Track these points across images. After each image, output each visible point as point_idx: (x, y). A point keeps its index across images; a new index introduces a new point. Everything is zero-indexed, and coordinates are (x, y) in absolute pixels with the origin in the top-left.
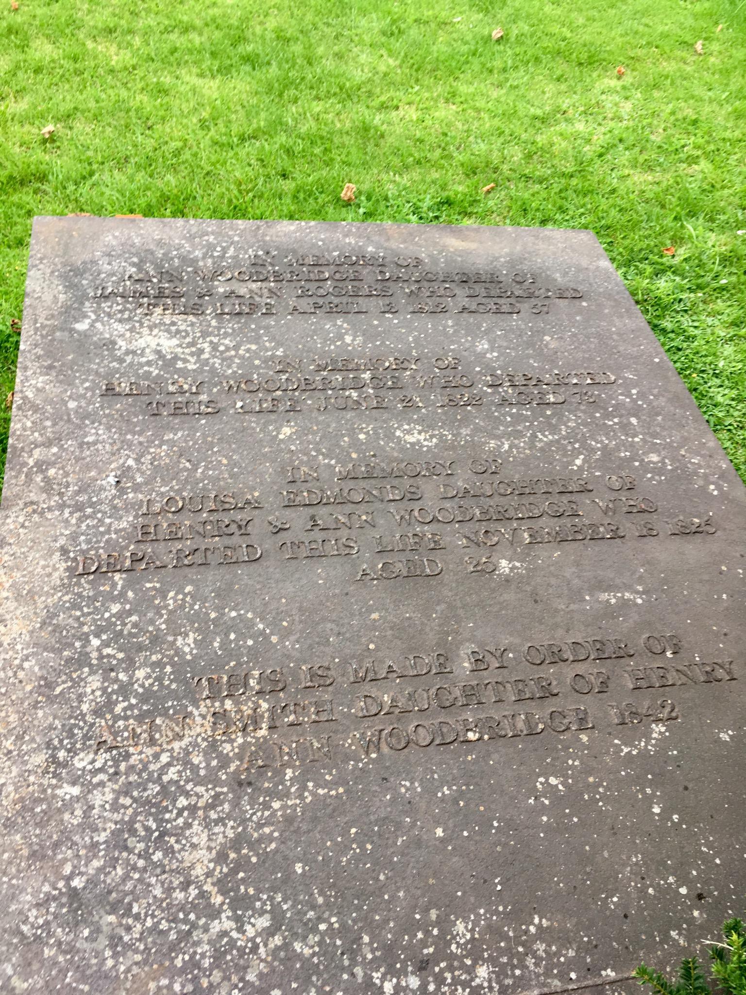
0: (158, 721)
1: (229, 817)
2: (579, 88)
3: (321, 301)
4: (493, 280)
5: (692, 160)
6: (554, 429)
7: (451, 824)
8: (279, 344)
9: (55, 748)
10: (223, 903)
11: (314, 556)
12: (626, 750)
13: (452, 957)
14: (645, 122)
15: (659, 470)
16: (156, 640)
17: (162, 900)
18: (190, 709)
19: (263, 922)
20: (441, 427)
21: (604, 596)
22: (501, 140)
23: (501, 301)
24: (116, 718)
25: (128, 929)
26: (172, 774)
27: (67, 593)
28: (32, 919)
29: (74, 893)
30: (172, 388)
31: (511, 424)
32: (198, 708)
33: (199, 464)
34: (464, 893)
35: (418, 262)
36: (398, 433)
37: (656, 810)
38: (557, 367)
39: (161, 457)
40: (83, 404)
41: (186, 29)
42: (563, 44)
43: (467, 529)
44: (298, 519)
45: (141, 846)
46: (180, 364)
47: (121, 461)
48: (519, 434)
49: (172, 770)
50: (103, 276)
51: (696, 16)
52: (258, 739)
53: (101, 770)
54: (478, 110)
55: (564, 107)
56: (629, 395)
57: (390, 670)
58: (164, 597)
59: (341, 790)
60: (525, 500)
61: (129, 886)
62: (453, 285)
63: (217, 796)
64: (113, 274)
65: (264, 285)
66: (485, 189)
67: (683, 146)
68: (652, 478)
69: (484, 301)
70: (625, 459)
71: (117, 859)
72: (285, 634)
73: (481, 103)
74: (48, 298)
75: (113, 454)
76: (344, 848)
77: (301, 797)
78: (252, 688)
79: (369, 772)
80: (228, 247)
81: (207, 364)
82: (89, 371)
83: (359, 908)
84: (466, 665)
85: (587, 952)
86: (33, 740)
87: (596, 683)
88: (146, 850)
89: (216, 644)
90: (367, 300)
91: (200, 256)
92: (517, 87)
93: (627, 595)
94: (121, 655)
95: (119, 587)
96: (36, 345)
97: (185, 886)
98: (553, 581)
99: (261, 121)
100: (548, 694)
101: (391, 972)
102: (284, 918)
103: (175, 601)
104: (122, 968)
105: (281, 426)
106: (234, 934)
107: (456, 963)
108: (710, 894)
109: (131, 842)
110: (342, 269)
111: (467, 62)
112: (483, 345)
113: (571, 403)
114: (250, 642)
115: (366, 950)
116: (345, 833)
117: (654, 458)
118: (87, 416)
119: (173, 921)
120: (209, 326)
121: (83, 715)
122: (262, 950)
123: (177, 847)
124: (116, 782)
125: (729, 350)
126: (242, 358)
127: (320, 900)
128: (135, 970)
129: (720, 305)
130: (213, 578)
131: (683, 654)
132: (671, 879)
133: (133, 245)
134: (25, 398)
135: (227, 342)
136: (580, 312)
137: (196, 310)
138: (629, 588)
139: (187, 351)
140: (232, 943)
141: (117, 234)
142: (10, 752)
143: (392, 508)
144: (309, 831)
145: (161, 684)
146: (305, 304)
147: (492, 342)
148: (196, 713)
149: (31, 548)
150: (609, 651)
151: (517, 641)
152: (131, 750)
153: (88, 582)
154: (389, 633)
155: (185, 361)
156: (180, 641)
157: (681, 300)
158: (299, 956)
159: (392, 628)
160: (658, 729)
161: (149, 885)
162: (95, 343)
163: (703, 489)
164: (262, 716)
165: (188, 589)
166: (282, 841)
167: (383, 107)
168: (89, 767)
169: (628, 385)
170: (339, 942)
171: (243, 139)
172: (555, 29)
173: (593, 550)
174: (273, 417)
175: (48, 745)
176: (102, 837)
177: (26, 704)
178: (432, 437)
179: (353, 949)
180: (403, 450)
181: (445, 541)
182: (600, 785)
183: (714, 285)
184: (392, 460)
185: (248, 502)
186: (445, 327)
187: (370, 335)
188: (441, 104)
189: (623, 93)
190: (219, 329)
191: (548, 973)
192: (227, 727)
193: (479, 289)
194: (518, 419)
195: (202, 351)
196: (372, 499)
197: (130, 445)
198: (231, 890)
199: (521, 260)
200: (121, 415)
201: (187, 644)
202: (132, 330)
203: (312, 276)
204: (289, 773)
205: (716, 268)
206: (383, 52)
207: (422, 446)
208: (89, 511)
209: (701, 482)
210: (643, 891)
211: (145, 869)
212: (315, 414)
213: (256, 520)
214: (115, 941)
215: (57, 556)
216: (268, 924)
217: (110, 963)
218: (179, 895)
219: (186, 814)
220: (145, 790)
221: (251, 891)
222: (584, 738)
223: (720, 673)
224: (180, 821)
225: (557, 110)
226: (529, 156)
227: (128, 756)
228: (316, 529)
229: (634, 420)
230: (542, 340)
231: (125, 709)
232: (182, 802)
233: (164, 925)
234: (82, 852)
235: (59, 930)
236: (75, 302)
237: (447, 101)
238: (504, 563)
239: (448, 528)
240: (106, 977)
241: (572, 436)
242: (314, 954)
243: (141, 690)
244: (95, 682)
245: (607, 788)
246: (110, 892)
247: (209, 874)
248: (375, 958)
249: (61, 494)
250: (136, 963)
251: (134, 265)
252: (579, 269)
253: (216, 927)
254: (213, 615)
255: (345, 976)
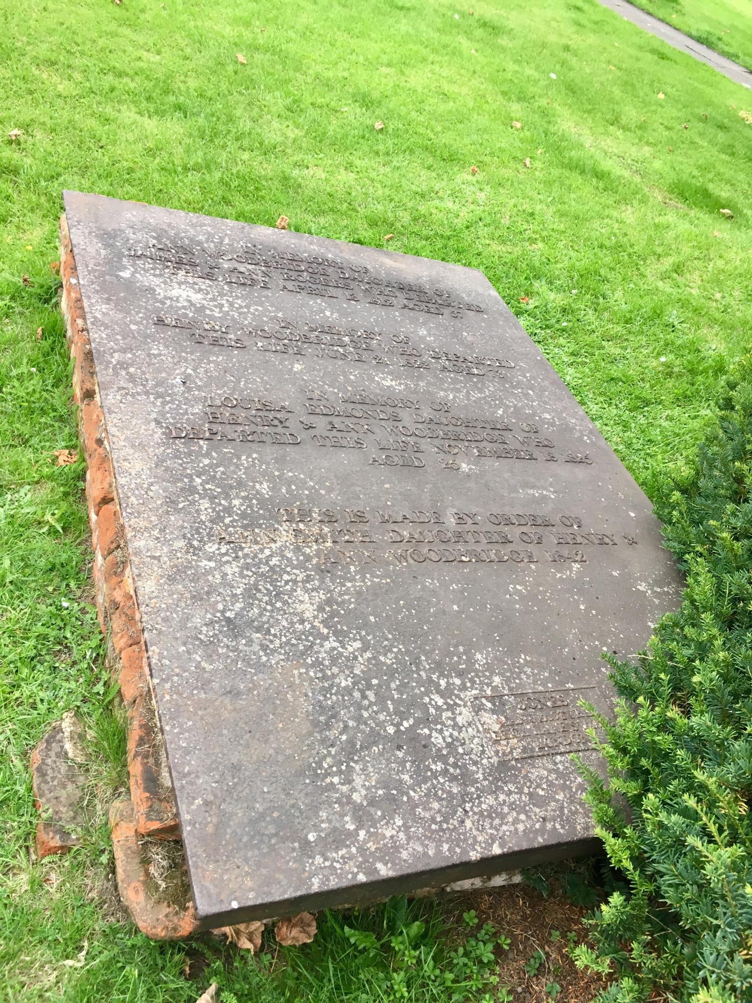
0: (256, 530)
1: (319, 587)
2: (445, 177)
3: (302, 285)
4: (421, 291)
5: (532, 241)
6: (481, 391)
7: (462, 603)
8: (278, 309)
9: (189, 539)
10: (329, 633)
11: (338, 446)
12: (559, 575)
13: (477, 671)
14: (496, 209)
15: (553, 424)
16: (241, 484)
17: (289, 629)
18: (276, 526)
19: (358, 645)
20: (405, 379)
21: (531, 491)
22: (393, 204)
23: (430, 305)
24: (227, 526)
25: (271, 642)
26: (274, 561)
27: (168, 448)
28: (204, 632)
29: (228, 620)
30: (207, 327)
31: (452, 383)
32: (282, 526)
33: (240, 379)
34: (477, 640)
35: (366, 271)
36: (376, 379)
37: (582, 607)
38: (475, 353)
39: (211, 371)
40: (142, 327)
41: (120, 75)
42: (429, 143)
43: (437, 442)
44: (321, 424)
45: (266, 598)
46: (208, 312)
47: (183, 369)
48: (459, 391)
49: (274, 559)
50: (132, 241)
51: (522, 140)
52: (327, 548)
53: (226, 554)
54: (373, 181)
55: (436, 188)
56: (525, 377)
57: (405, 518)
58: (239, 459)
59: (388, 580)
60: (472, 430)
61: (265, 619)
62: (394, 290)
63: (308, 576)
64: (140, 242)
65: (257, 267)
66: (386, 237)
67: (525, 230)
68: (548, 428)
69: (417, 303)
70: (529, 414)
71: (252, 604)
72: (330, 490)
73: (373, 175)
74: (91, 250)
75: (175, 364)
76: (399, 611)
77: (363, 581)
78: (315, 519)
79: (403, 572)
80: (224, 237)
81: (229, 315)
82: (140, 307)
83: (414, 642)
84: (452, 520)
85: (556, 674)
86: (172, 533)
87: (535, 539)
88: (271, 600)
89: (284, 491)
90: (335, 289)
91: (204, 240)
92: (398, 168)
93: (545, 492)
94: (219, 490)
95: (205, 449)
96: (93, 283)
97: (302, 621)
98: (498, 479)
99: (198, 157)
100: (507, 541)
101: (442, 675)
102: (370, 643)
103: (248, 462)
104: (273, 662)
105: (294, 363)
106: (340, 649)
107: (480, 674)
108: (621, 652)
109: (259, 595)
110: (312, 266)
111: (358, 143)
112: (423, 332)
113: (488, 376)
114: (307, 492)
115: (425, 663)
116: (397, 602)
117: (548, 416)
118: (147, 337)
119: (299, 639)
120: (223, 289)
121: (204, 523)
122: (360, 658)
123: (290, 601)
124: (239, 562)
125: (571, 371)
126: (253, 314)
127: (390, 636)
128: (282, 663)
129: (562, 341)
130: (271, 452)
131: (583, 528)
132: (597, 643)
133: (149, 224)
134: (95, 317)
135: (239, 301)
136: (483, 320)
137: (209, 276)
138: (545, 488)
139: (211, 303)
140: (341, 655)
141: (134, 213)
142: (157, 538)
143: (383, 423)
144: (373, 600)
145: (252, 510)
146: (290, 285)
147: (429, 331)
148: (281, 529)
149: (132, 417)
150: (539, 522)
151: (482, 510)
152: (243, 545)
153: (182, 443)
154: (399, 497)
155: (211, 310)
156: (258, 486)
157: (535, 334)
158: (384, 664)
159: (400, 494)
160: (576, 566)
161: (278, 620)
162: (139, 288)
163: (580, 438)
164: (326, 535)
165: (255, 456)
166: (356, 602)
167: (296, 165)
168: (217, 552)
169: (523, 371)
170: (407, 658)
171: (186, 169)
172: (421, 130)
173: (519, 464)
174: (286, 356)
175: (184, 537)
176: (239, 591)
177: (160, 511)
178: (400, 384)
179: (416, 662)
180: (381, 389)
181: (423, 447)
182: (546, 592)
183: (557, 326)
184: (376, 395)
185: (283, 408)
186: (394, 316)
187: (343, 313)
188: (342, 170)
189: (478, 186)
190: (231, 292)
191: (535, 683)
192: (305, 538)
193: (412, 295)
194: (455, 381)
195: (223, 305)
196: (368, 416)
197: (186, 360)
198: (332, 626)
199: (439, 282)
200: (173, 339)
201: (264, 488)
202: (165, 283)
203: (292, 267)
204: (352, 568)
205: (559, 315)
206: (290, 123)
207: (395, 389)
208: (168, 399)
209: (578, 434)
210: (582, 647)
211: (272, 611)
212: (315, 358)
213: (291, 420)
214: (264, 648)
215: (153, 424)
216: (360, 646)
217: (264, 659)
218: (299, 627)
219: (290, 584)
220: (260, 568)
221: (345, 628)
222: (533, 567)
223: (607, 540)
224: (288, 587)
225: (432, 190)
226: (415, 219)
227: (242, 549)
228: (335, 430)
229: (530, 392)
230: (462, 335)
231: (231, 521)
232: (286, 577)
233: (294, 641)
234: (228, 598)
235: (225, 639)
236: (114, 257)
237: (346, 168)
238: (464, 465)
239: (423, 440)
240: (264, 666)
241: (493, 396)
242: (393, 663)
243: (239, 512)
244: (205, 504)
245: (551, 594)
246: (253, 621)
247: (315, 617)
248: (430, 668)
249: (144, 386)
250: (282, 660)
251: (154, 238)
252: (478, 294)
253: (327, 645)
254: (277, 473)
255: (415, 676)
